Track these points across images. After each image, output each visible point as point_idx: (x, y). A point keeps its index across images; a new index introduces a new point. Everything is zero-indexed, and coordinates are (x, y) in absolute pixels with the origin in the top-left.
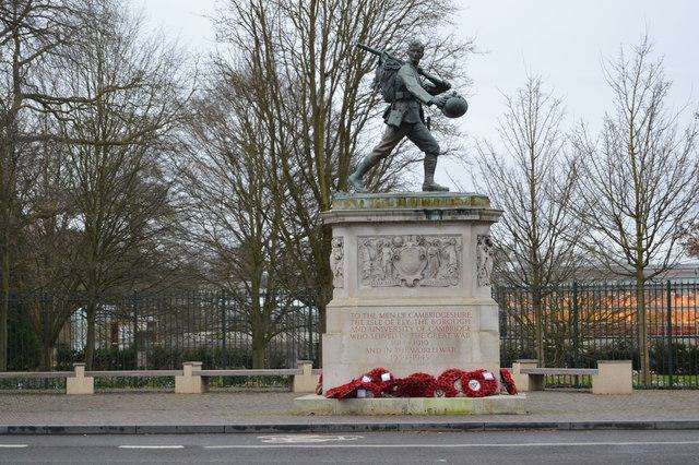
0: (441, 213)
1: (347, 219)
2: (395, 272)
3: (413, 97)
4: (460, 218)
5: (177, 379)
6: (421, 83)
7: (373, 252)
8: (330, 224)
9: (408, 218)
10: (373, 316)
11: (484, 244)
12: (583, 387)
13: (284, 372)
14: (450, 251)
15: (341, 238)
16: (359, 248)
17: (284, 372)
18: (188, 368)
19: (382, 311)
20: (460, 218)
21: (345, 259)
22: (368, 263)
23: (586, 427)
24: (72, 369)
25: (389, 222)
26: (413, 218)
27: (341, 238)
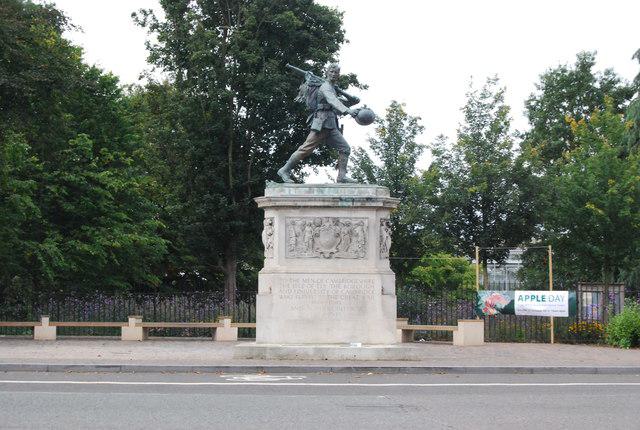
0: (353, 200)
1: (278, 204)
2: (316, 247)
3: (330, 108)
4: (367, 204)
5: (36, 328)
6: (341, 100)
7: (298, 229)
8: (265, 207)
9: (326, 204)
10: (297, 280)
11: (385, 226)
12: (447, 337)
13: (211, 325)
14: (358, 230)
15: (272, 219)
16: (287, 226)
17: (211, 325)
18: (132, 320)
19: (306, 277)
20: (367, 204)
21: (276, 235)
22: (294, 239)
23: (507, 371)
24: (127, 321)
25: (311, 207)
26: (330, 204)
27: (272, 219)
